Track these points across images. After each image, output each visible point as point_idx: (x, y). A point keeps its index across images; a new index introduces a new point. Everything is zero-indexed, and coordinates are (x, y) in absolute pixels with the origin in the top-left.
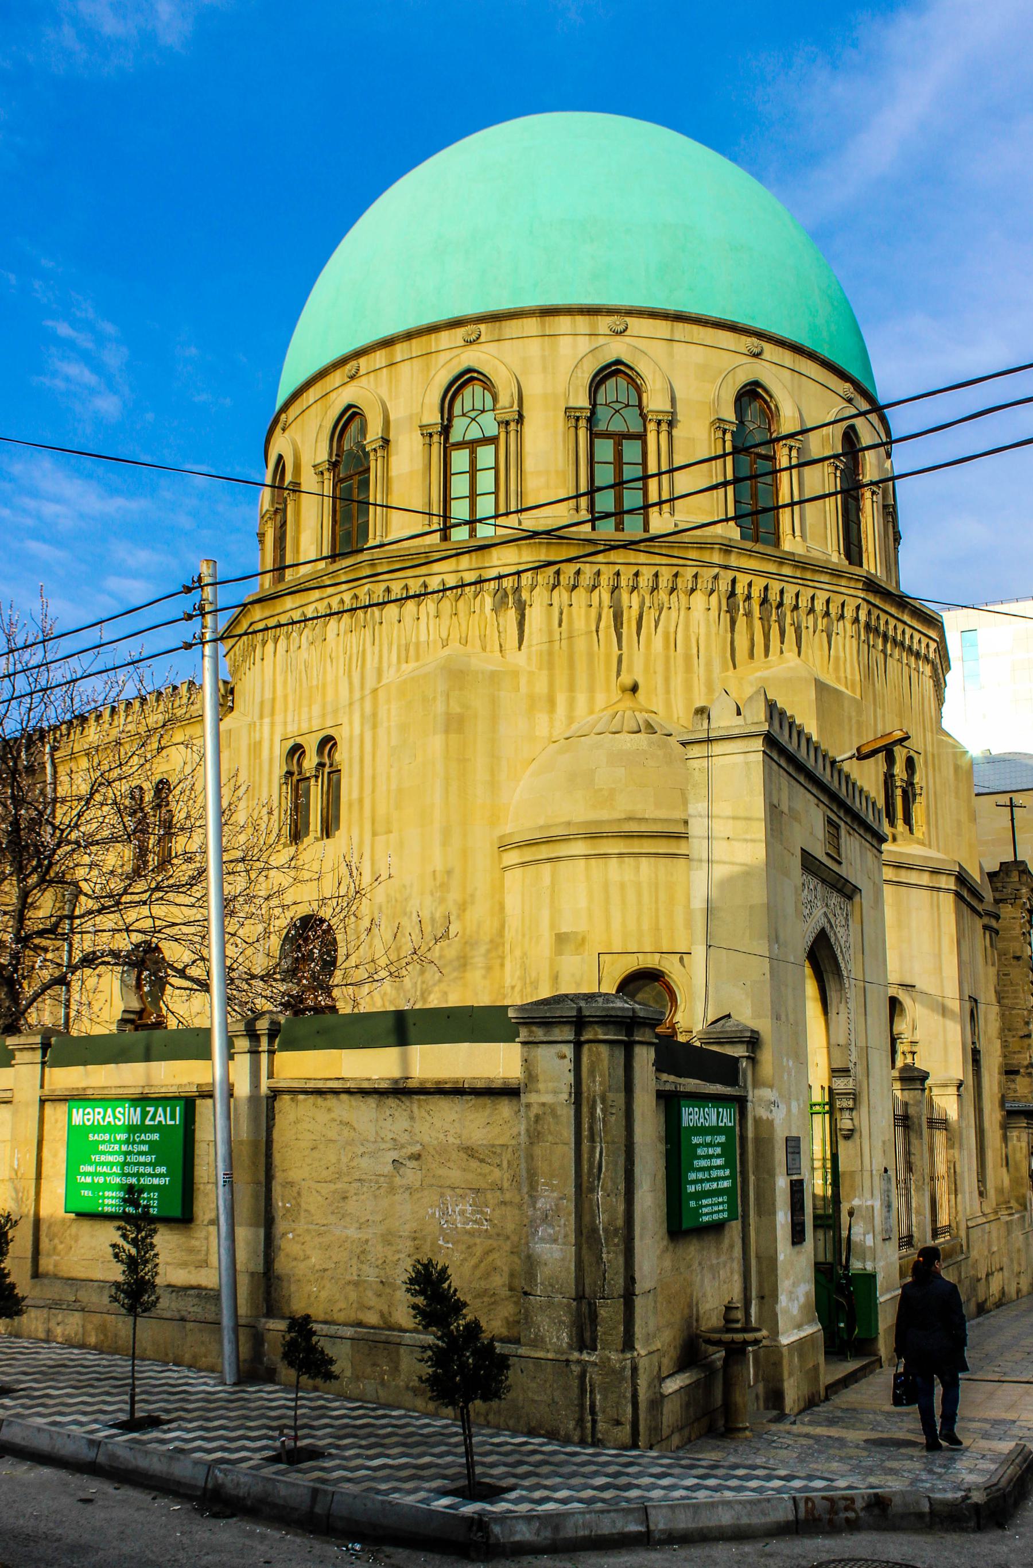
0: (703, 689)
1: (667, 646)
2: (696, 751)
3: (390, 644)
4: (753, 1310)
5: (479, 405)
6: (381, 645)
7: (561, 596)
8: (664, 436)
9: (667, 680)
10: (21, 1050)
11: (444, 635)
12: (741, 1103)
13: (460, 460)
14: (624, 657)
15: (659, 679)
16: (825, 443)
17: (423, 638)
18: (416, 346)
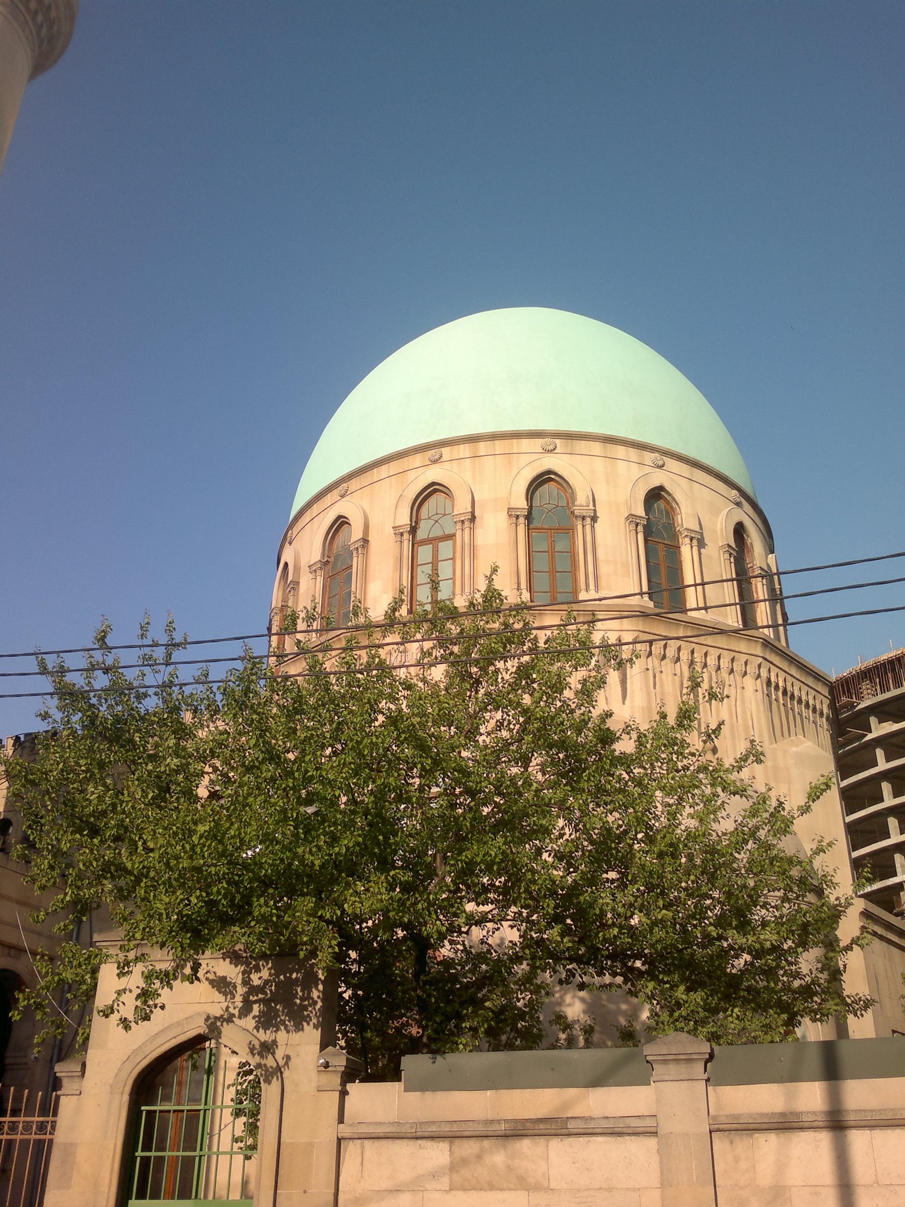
7: (653, 662)
8: (588, 528)
10: (665, 1062)
16: (719, 533)
18: (394, 467)
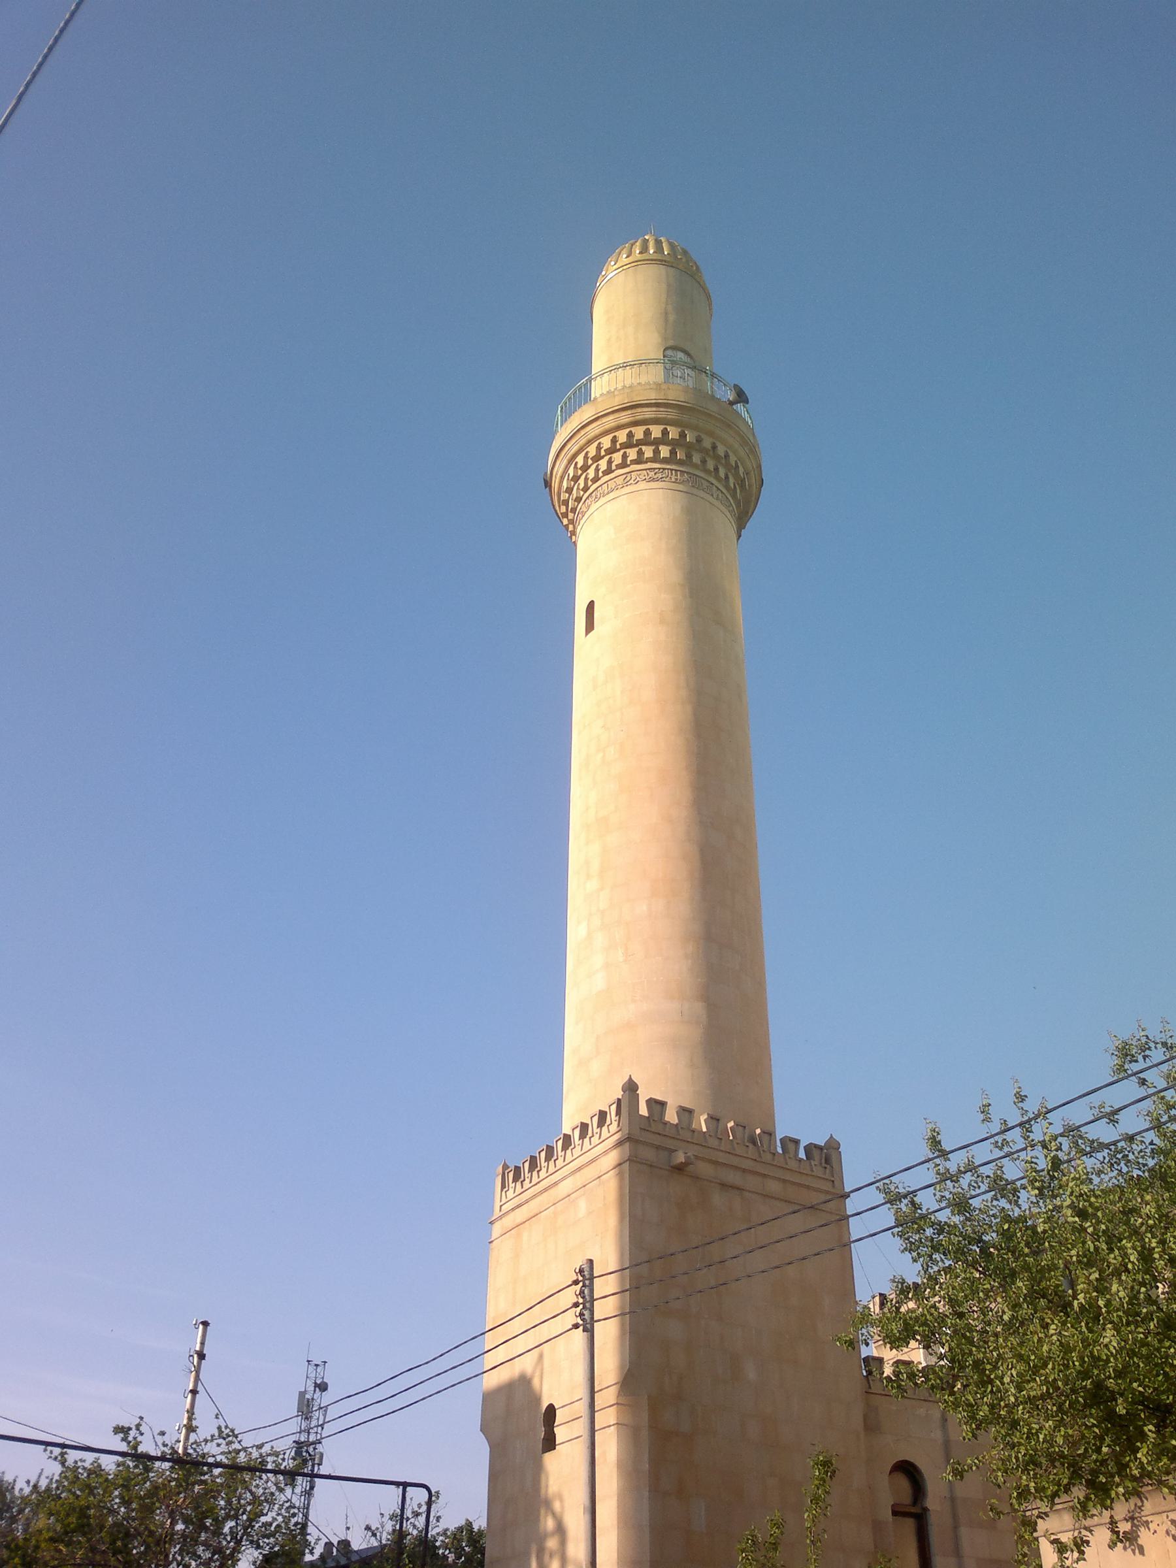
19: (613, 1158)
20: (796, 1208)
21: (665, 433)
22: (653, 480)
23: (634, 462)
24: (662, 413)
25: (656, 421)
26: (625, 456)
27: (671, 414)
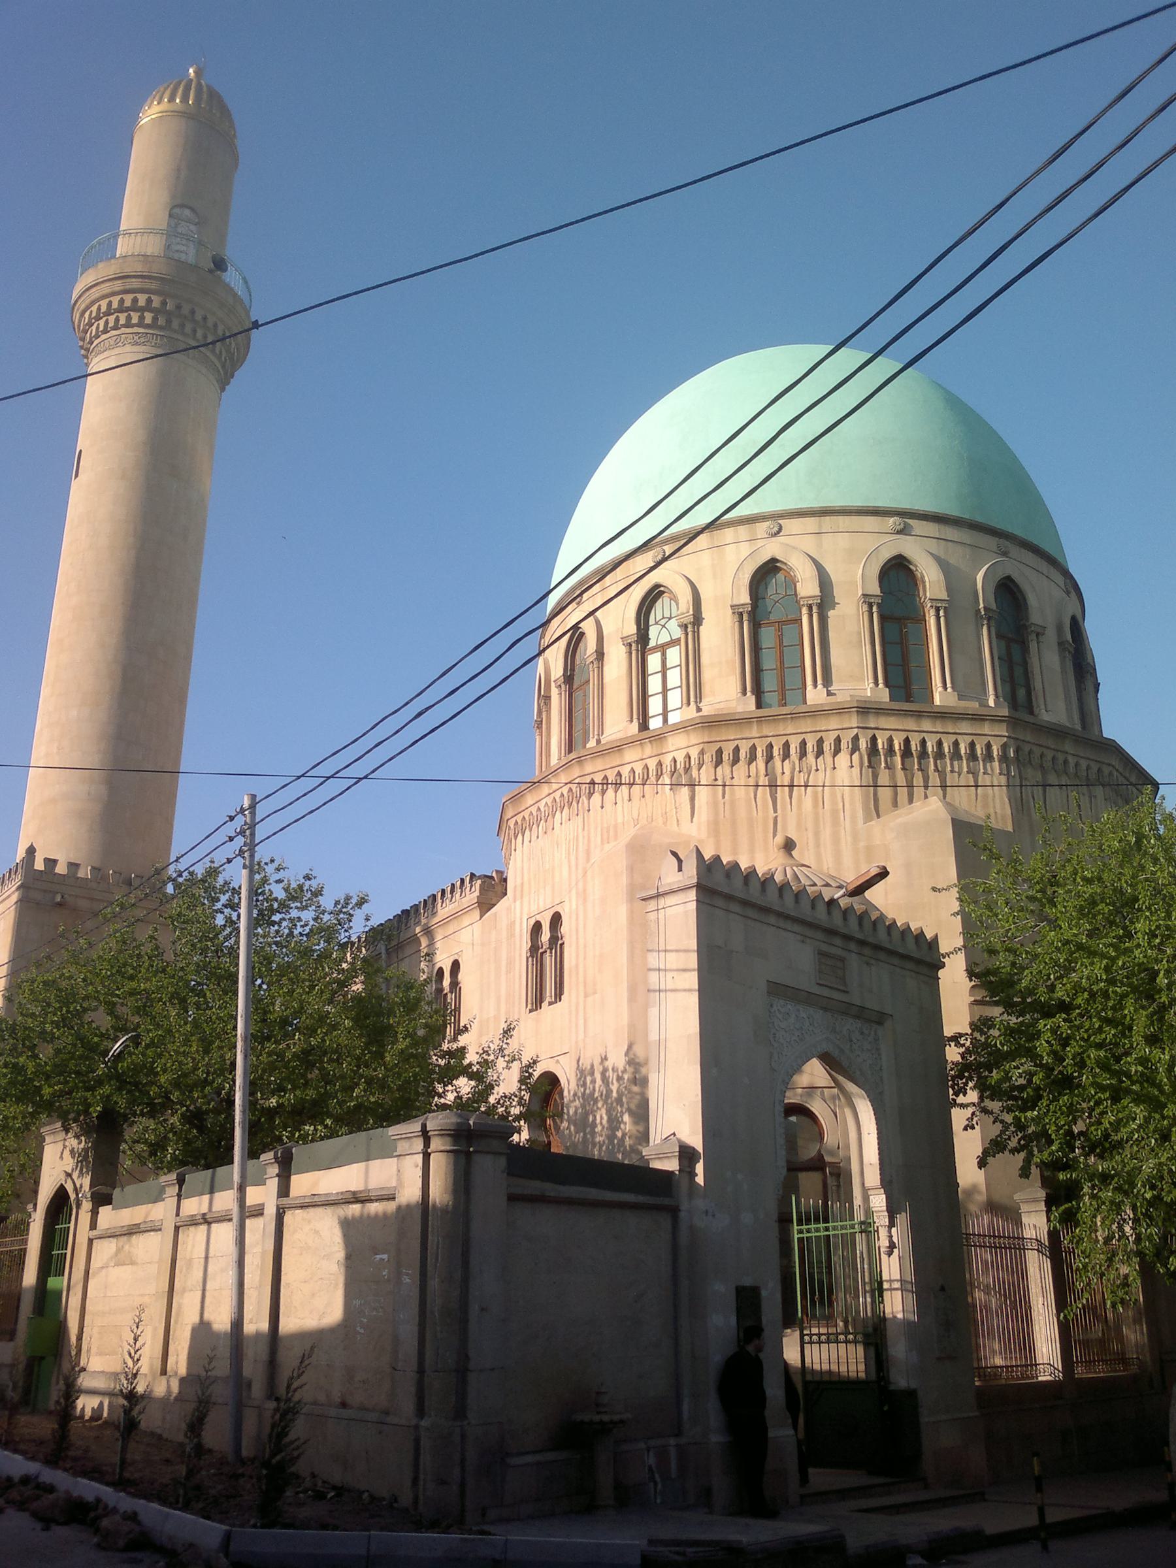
0: (849, 839)
1: (815, 805)
2: (652, 905)
3: (596, 828)
4: (685, 1407)
5: (667, 614)
6: (589, 830)
9: (817, 834)
11: (635, 816)
12: (674, 1211)
13: (654, 661)
14: (779, 819)
15: (810, 835)
17: (620, 820)
19: (15, 898)
20: (516, 788)
21: (149, 301)
22: (136, 344)
23: (123, 326)
24: (147, 284)
25: (142, 291)
26: (117, 319)
27: (152, 285)
